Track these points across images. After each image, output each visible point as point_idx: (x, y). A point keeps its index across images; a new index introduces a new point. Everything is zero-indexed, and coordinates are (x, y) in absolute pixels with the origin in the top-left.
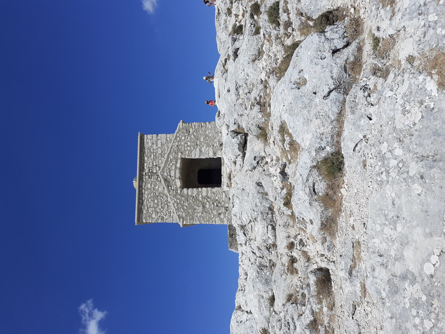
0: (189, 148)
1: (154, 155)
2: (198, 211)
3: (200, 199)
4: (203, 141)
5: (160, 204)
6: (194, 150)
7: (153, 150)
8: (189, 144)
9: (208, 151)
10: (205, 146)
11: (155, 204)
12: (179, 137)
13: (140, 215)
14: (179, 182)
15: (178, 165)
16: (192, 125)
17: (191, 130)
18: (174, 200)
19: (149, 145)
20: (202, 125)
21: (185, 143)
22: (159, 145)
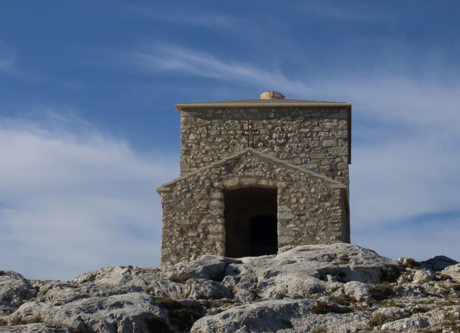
0: (294, 200)
1: (306, 134)
2: (183, 218)
3: (203, 221)
4: (307, 225)
5: (213, 147)
6: (289, 210)
7: (318, 132)
8: (302, 201)
9: (289, 235)
10: (297, 229)
11: (214, 139)
12: (315, 183)
13: (194, 111)
14: (234, 184)
15: (263, 182)
16: (337, 205)
17: (327, 204)
18: (202, 176)
19: (328, 123)
20: (336, 225)
21: (303, 193)
22: (325, 143)
